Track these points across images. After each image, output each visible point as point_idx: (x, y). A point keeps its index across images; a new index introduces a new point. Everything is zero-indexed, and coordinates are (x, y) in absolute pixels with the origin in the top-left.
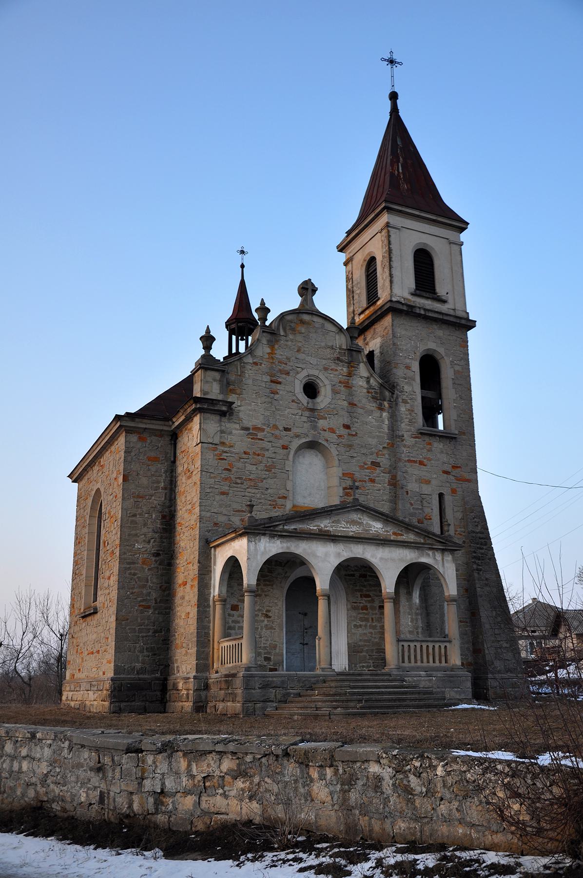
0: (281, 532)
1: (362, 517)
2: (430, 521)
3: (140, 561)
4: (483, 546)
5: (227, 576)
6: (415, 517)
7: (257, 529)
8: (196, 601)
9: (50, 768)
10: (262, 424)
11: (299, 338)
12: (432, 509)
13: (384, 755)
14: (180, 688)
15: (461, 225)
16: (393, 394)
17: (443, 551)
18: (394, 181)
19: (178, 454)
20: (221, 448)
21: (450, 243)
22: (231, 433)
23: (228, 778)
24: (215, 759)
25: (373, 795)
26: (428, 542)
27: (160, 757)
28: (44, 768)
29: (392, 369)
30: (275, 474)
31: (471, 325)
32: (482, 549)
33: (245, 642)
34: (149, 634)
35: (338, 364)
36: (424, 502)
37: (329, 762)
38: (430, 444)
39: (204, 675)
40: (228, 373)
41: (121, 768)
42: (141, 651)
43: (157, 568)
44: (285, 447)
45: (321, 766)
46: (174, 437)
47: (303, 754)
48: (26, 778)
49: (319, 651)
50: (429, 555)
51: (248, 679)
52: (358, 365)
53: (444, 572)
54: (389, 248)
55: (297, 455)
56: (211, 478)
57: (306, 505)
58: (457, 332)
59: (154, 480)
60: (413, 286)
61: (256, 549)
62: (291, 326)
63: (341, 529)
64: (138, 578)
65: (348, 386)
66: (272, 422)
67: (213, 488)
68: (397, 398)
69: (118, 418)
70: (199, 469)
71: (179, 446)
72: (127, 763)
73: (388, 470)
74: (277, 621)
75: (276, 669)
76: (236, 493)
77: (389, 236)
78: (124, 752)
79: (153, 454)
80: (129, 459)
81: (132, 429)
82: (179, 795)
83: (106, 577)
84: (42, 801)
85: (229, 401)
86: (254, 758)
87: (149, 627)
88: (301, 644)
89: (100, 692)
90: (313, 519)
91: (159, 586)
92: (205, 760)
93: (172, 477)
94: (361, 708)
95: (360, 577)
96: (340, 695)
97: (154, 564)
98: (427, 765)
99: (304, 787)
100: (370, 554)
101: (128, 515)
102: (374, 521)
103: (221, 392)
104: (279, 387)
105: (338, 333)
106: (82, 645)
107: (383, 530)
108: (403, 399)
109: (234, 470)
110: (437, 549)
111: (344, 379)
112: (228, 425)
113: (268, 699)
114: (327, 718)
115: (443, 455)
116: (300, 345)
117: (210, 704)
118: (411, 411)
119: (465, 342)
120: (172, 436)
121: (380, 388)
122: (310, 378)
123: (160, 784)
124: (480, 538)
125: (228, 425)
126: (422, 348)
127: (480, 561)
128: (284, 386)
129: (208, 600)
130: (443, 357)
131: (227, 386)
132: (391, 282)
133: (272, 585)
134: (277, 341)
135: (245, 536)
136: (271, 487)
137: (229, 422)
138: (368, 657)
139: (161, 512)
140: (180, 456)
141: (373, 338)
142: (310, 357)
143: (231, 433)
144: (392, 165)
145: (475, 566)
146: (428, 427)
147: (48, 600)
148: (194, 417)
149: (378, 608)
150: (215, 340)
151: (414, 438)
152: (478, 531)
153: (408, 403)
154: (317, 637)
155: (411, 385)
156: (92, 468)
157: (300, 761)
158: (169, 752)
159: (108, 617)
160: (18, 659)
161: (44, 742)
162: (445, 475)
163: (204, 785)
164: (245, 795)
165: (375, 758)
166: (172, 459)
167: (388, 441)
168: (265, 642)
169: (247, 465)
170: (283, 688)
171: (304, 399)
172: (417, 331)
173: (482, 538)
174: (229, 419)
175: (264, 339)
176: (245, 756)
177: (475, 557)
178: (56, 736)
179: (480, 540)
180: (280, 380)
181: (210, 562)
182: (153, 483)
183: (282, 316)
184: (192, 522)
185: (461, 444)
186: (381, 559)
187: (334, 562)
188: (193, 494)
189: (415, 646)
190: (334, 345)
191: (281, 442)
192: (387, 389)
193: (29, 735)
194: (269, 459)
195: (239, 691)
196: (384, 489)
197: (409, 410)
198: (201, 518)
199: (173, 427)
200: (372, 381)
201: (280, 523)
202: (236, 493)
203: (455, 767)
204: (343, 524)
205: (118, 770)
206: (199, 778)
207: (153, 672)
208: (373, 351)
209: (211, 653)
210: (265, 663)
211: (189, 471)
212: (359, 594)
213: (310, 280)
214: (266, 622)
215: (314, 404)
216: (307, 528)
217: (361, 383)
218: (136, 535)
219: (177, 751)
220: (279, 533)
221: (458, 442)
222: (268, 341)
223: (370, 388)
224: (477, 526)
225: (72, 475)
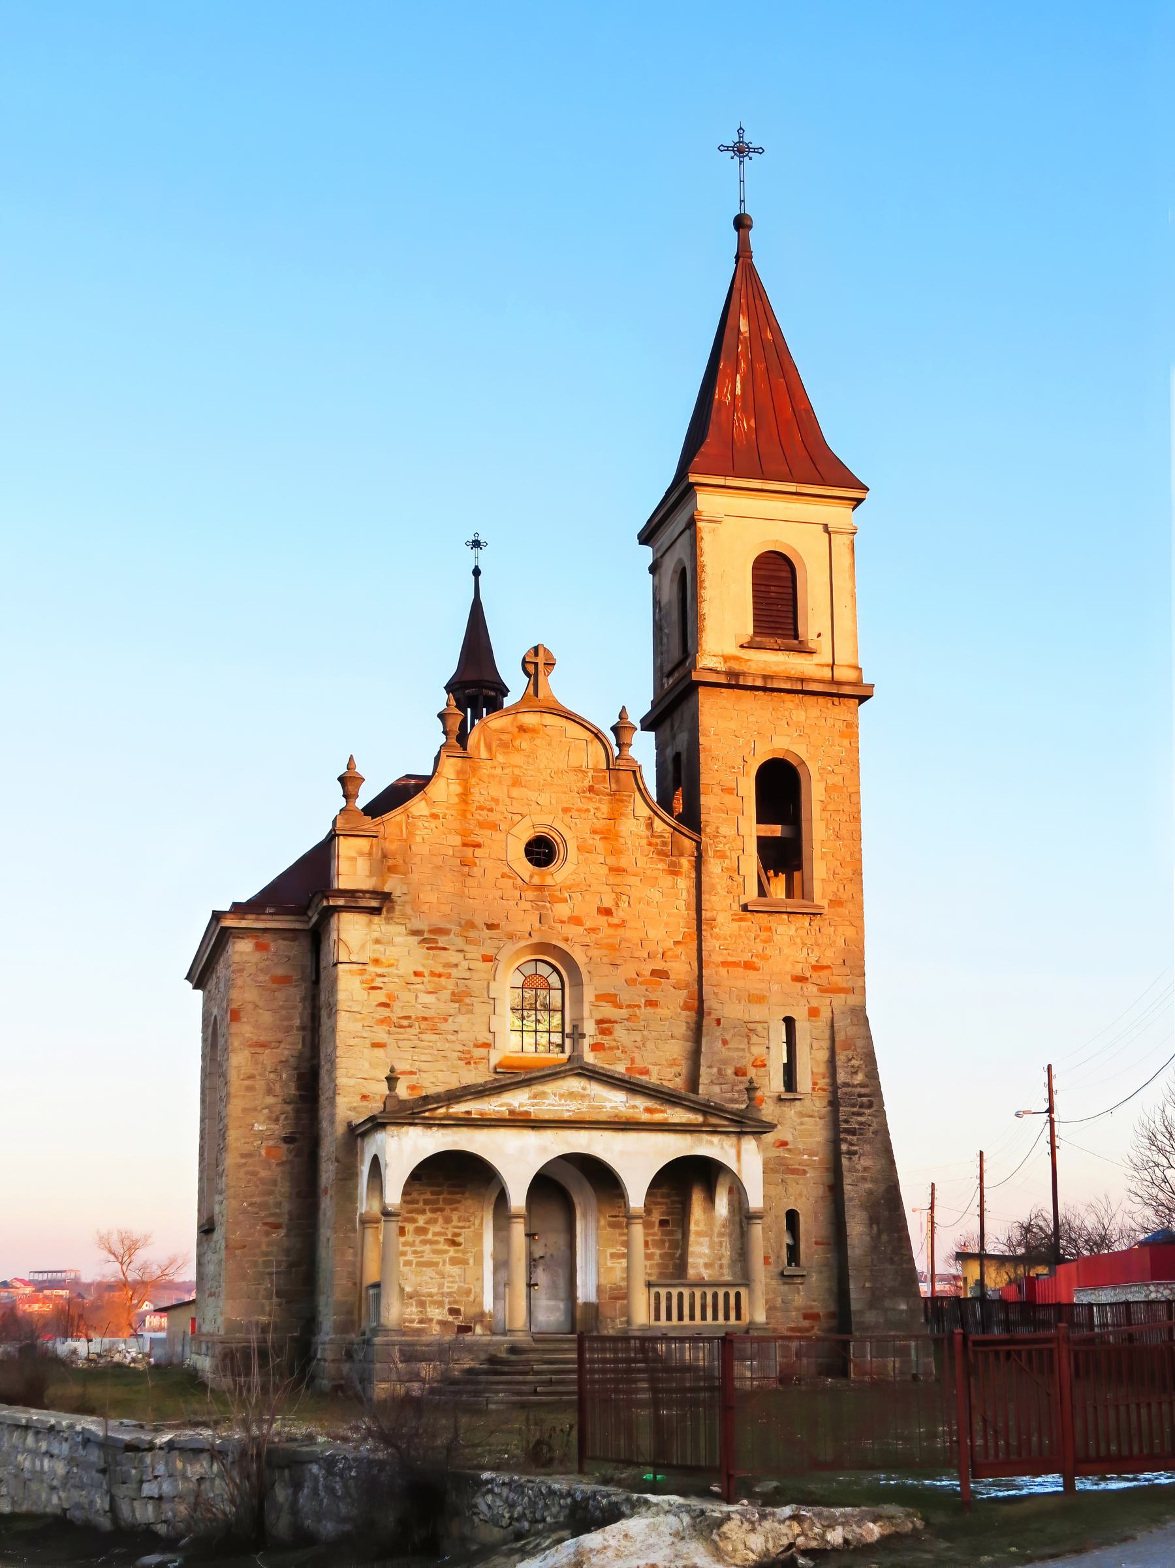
2: (763, 1069)
11: (517, 759)
20: (372, 969)
22: (391, 943)
35: (590, 799)
42: (269, 1297)
50: (711, 1143)
53: (739, 1170)
56: (356, 1020)
60: (747, 628)
62: (501, 740)
65: (609, 835)
101: (242, 1077)
111: (600, 824)
119: (851, 730)
124: (860, 1096)
127: (855, 1138)
137: (387, 923)
149: (657, 1224)
152: (856, 1082)
161: (61, 1434)
162: (799, 985)
168: (450, 1285)
171: (525, 867)
180: (481, 841)
194: (459, 981)
197: (727, 869)
210: (451, 1318)
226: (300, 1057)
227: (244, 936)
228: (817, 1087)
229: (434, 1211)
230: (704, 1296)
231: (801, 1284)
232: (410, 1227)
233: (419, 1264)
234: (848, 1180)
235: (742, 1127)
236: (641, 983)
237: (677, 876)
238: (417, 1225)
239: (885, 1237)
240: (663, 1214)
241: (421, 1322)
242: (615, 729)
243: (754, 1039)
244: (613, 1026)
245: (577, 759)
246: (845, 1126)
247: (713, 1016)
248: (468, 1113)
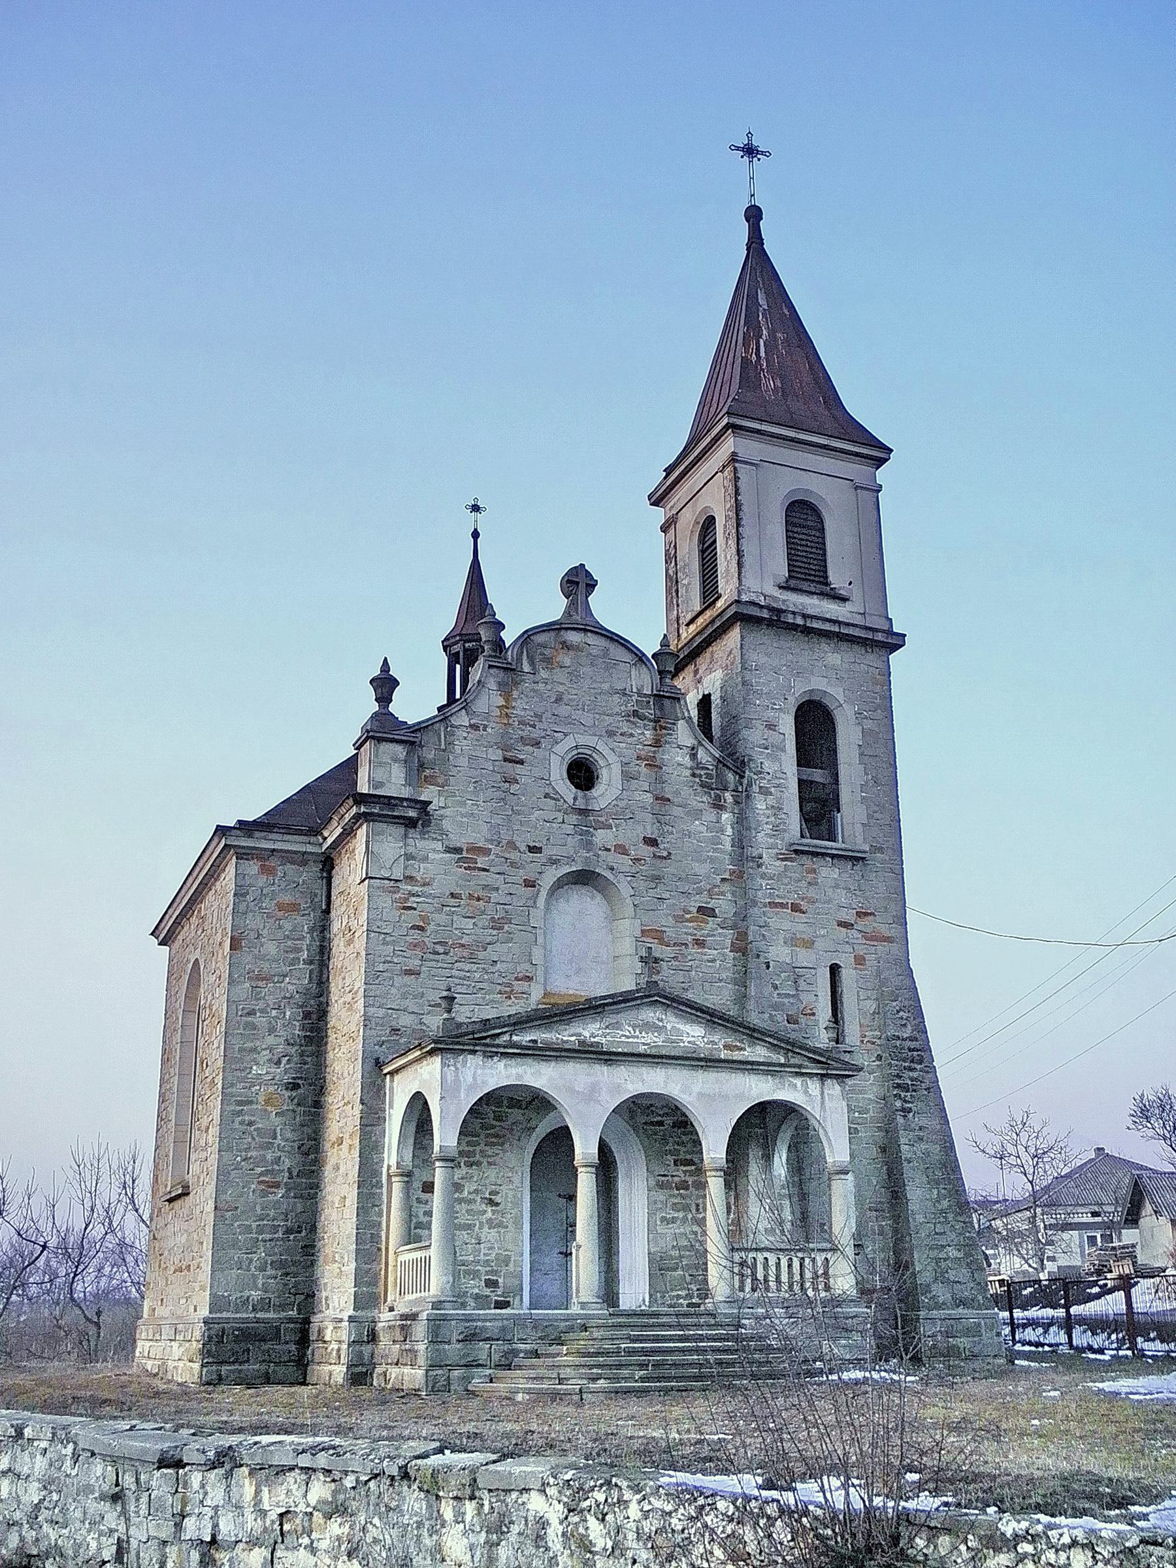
0: (504, 1047)
1: (664, 1017)
2: (812, 1017)
3: (261, 1099)
4: (916, 1065)
5: (412, 1128)
6: (782, 1010)
7: (458, 1043)
8: (356, 1175)
9: (43, 1493)
10: (487, 840)
11: (560, 676)
12: (816, 995)
13: (552, 1481)
14: (327, 1338)
15: (878, 455)
16: (742, 777)
17: (823, 1077)
18: (749, 374)
19: (333, 898)
21: (856, 488)
22: (425, 859)
23: (318, 1517)
24: (298, 1480)
25: (534, 1551)
26: (792, 1061)
27: (213, 1477)
28: (33, 1494)
29: (739, 731)
30: (510, 933)
31: (894, 642)
33: (434, 1253)
34: (276, 1236)
35: (634, 723)
36: (801, 982)
37: (468, 1491)
38: (814, 871)
39: (369, 1315)
40: (421, 746)
41: (150, 1495)
42: (262, 1269)
43: (294, 1111)
44: (530, 884)
45: (456, 1498)
46: (328, 864)
47: (429, 1476)
48: (6, 1512)
49: (578, 1272)
51: (437, 1325)
52: (674, 724)
54: (736, 499)
55: (553, 898)
56: (385, 943)
57: (571, 992)
59: (290, 947)
60: (782, 569)
61: (457, 1080)
63: (623, 1039)
64: (257, 1129)
65: (654, 765)
66: (505, 837)
67: (390, 962)
68: (750, 785)
69: (240, 822)
70: (365, 928)
71: (335, 882)
72: (160, 1486)
73: (730, 923)
74: (512, 1211)
75: (509, 1302)
77: (736, 479)
78: (155, 1467)
79: (287, 898)
81: (248, 851)
82: (241, 1546)
83: (203, 1128)
84: (30, 1556)
85: (422, 798)
86: (357, 1481)
87: (275, 1223)
88: (561, 1253)
89: (187, 1345)
90: (569, 1022)
91: (296, 1145)
92: (282, 1484)
93: (323, 939)
94: (643, 1380)
95: (673, 1127)
96: (606, 1354)
97: (288, 1106)
98: (615, 1500)
99: (431, 1535)
101: (240, 1013)
103: (408, 783)
106: (166, 1253)
107: (706, 1040)
108: (760, 787)
109: (430, 928)
110: (810, 1075)
112: (419, 844)
113: (474, 1361)
114: (576, 1398)
116: (561, 688)
117: (379, 1370)
118: (777, 809)
120: (324, 863)
121: (717, 767)
122: (580, 751)
123: (210, 1525)
124: (910, 1050)
125: (420, 844)
126: (799, 690)
129: (376, 1173)
131: (419, 771)
132: (740, 565)
133: (502, 1144)
134: (516, 684)
135: (437, 1055)
138: (688, 1278)
139: (301, 1007)
140: (336, 901)
141: (710, 670)
142: (581, 712)
143: (425, 859)
144: (746, 344)
145: (898, 1104)
146: (811, 838)
147: (134, 1162)
148: (357, 829)
150: (398, 684)
151: (783, 860)
152: (905, 1036)
154: (574, 1244)
155: (774, 758)
156: (188, 919)
157: (425, 1488)
158: (227, 1467)
159: (203, 1200)
160: (76, 1275)
161: (36, 1444)
163: (281, 1529)
164: (343, 1548)
165: (538, 1485)
166: (324, 907)
167: (731, 867)
169: (455, 918)
170: (504, 1341)
171: (567, 791)
174: (423, 833)
175: (492, 680)
176: (344, 1476)
177: (899, 1086)
178: (54, 1434)
180: (522, 757)
181: (384, 1102)
182: (287, 952)
183: (527, 637)
184: (353, 1028)
186: (701, 1095)
188: (355, 974)
189: (766, 1259)
191: (522, 874)
192: (730, 769)
193: (13, 1430)
195: (421, 1347)
196: (722, 958)
198: (367, 1019)
199: (325, 846)
200: (701, 753)
201: (504, 1030)
203: (657, 1504)
204: (628, 1030)
205: (144, 1499)
206: (273, 1516)
207: (282, 1307)
208: (710, 695)
209: (383, 1272)
211: (350, 930)
213: (582, 566)
214: (489, 1215)
215: (587, 800)
216: (557, 1039)
217: (679, 759)
218: (254, 1050)
219: (241, 1466)
220: (502, 1050)
221: (869, 867)
222: (501, 685)
223: (698, 768)
224: (905, 1025)
225: (157, 932)
226: (306, 993)
228: (866, 1040)
229: (470, 1165)
247: (762, 959)
248: (535, 1041)
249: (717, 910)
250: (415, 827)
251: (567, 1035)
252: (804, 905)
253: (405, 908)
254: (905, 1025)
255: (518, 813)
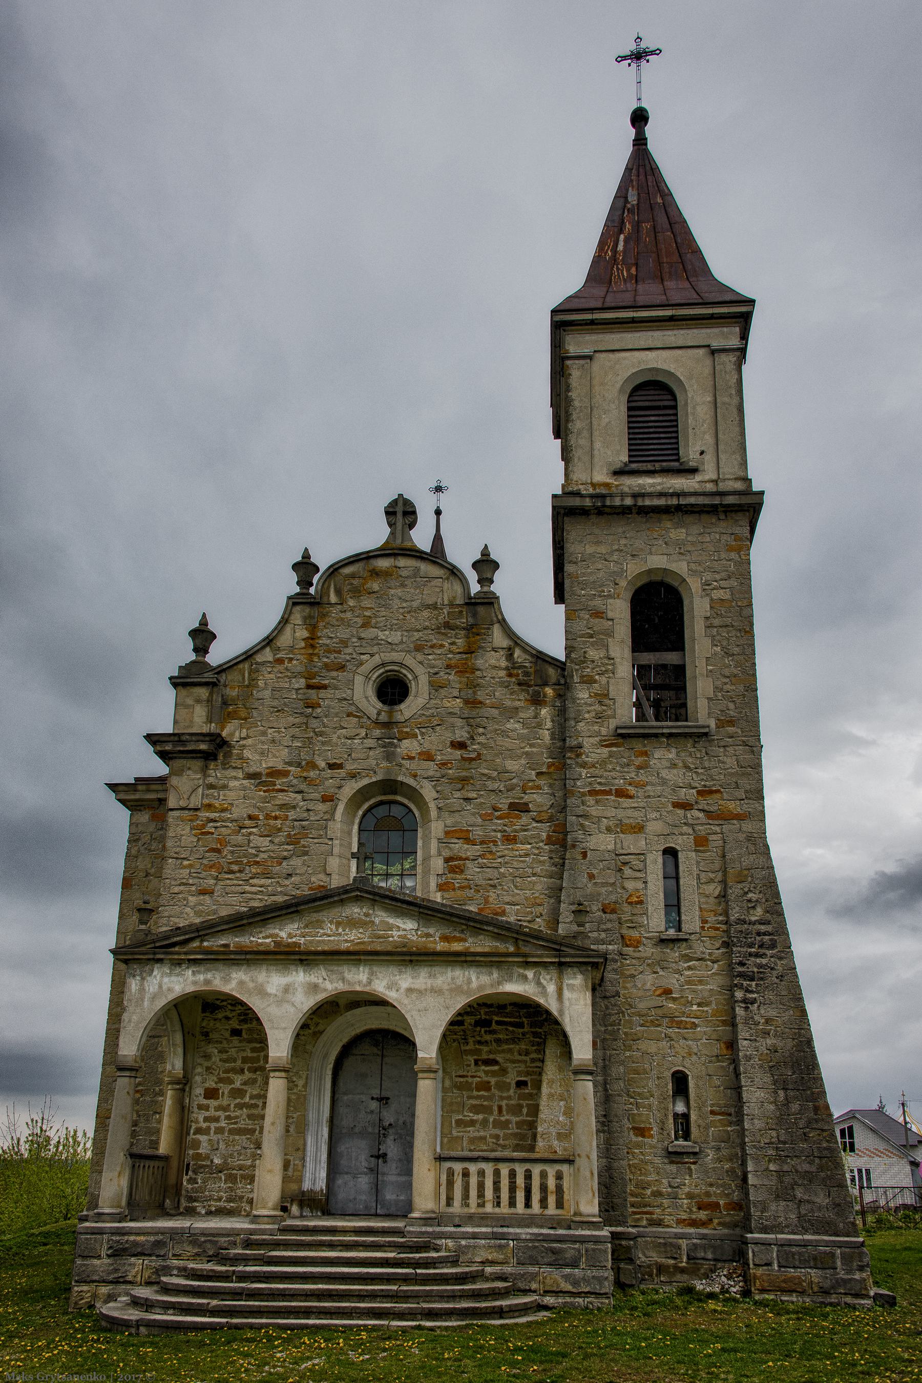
1: (371, 912)
6: (597, 900)
10: (286, 763)
21: (713, 352)
22: (225, 787)
32: (761, 956)
35: (443, 634)
38: (645, 754)
50: (525, 978)
52: (489, 629)
53: (561, 1011)
58: (723, 524)
61: (142, 990)
65: (466, 670)
73: (545, 816)
76: (228, 889)
80: (134, 852)
88: (372, 1156)
100: (384, 983)
102: (398, 917)
104: (322, 693)
105: (448, 579)
112: (216, 774)
115: (675, 771)
124: (759, 934)
126: (633, 568)
127: (754, 983)
128: (333, 691)
130: (685, 580)
134: (324, 616)
136: (298, 872)
149: (513, 1085)
151: (606, 746)
152: (753, 919)
153: (595, 682)
162: (680, 812)
171: (372, 705)
172: (623, 542)
173: (765, 934)
179: (758, 938)
180: (326, 682)
185: (722, 744)
186: (410, 990)
187: (302, 1003)
190: (439, 601)
197: (596, 694)
202: (228, 889)
204: (330, 928)
212: (471, 1059)
215: (390, 713)
216: (251, 942)
217: (493, 662)
223: (513, 668)
224: (754, 908)
227: (142, 808)
230: (512, 1174)
231: (694, 1163)
232: (225, 1089)
233: (231, 1132)
234: (743, 1033)
235: (560, 956)
236: (498, 818)
237: (540, 705)
238: (233, 1086)
239: (795, 1107)
240: (519, 1073)
241: (229, 1200)
242: (475, 565)
243: (628, 872)
244: (464, 865)
245: (430, 595)
246: (741, 969)
249: (530, 805)
250: (216, 759)
251: (261, 938)
252: (632, 790)
253: (203, 834)
254: (754, 908)
255: (321, 734)
